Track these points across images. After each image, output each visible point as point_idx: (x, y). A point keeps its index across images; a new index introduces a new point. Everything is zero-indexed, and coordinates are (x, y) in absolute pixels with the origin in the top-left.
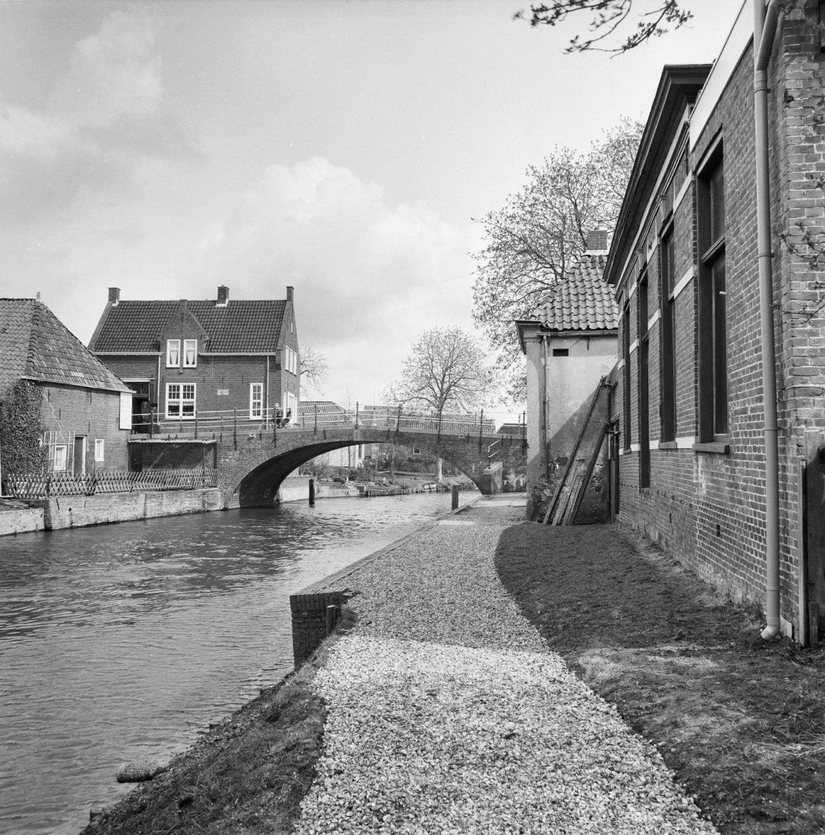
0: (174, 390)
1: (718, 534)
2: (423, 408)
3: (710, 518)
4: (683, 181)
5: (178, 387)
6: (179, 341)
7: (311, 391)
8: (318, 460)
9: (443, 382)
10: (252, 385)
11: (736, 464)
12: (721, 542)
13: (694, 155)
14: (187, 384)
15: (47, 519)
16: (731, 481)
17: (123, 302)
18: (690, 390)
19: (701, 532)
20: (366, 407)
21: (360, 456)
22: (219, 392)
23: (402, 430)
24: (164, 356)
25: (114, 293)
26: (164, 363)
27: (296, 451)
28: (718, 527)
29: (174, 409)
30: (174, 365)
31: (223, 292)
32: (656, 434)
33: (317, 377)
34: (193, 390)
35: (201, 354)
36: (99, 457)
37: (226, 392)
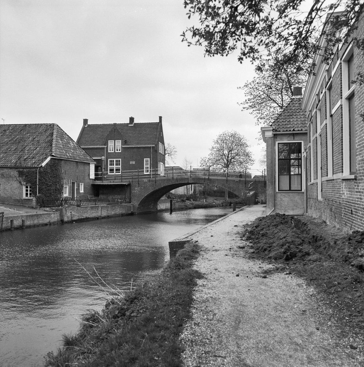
0: (112, 162)
1: (352, 214)
2: (219, 168)
3: (348, 207)
4: (336, 63)
5: (113, 161)
6: (114, 141)
7: (170, 162)
8: (173, 191)
9: (228, 157)
10: (145, 159)
11: (359, 183)
12: (352, 217)
13: (341, 51)
14: (111, 159)
15: (61, 215)
16: (357, 190)
17: (89, 125)
18: (339, 153)
19: (344, 214)
20: (193, 169)
21: (192, 190)
22: (131, 163)
23: (210, 177)
24: (107, 148)
25: (86, 121)
26: (107, 150)
27: (165, 187)
28: (352, 211)
29: (112, 170)
30: (111, 152)
31: (132, 119)
32: (324, 174)
33: (172, 156)
34: (120, 162)
35: (123, 146)
36: (82, 191)
37: (134, 163)
